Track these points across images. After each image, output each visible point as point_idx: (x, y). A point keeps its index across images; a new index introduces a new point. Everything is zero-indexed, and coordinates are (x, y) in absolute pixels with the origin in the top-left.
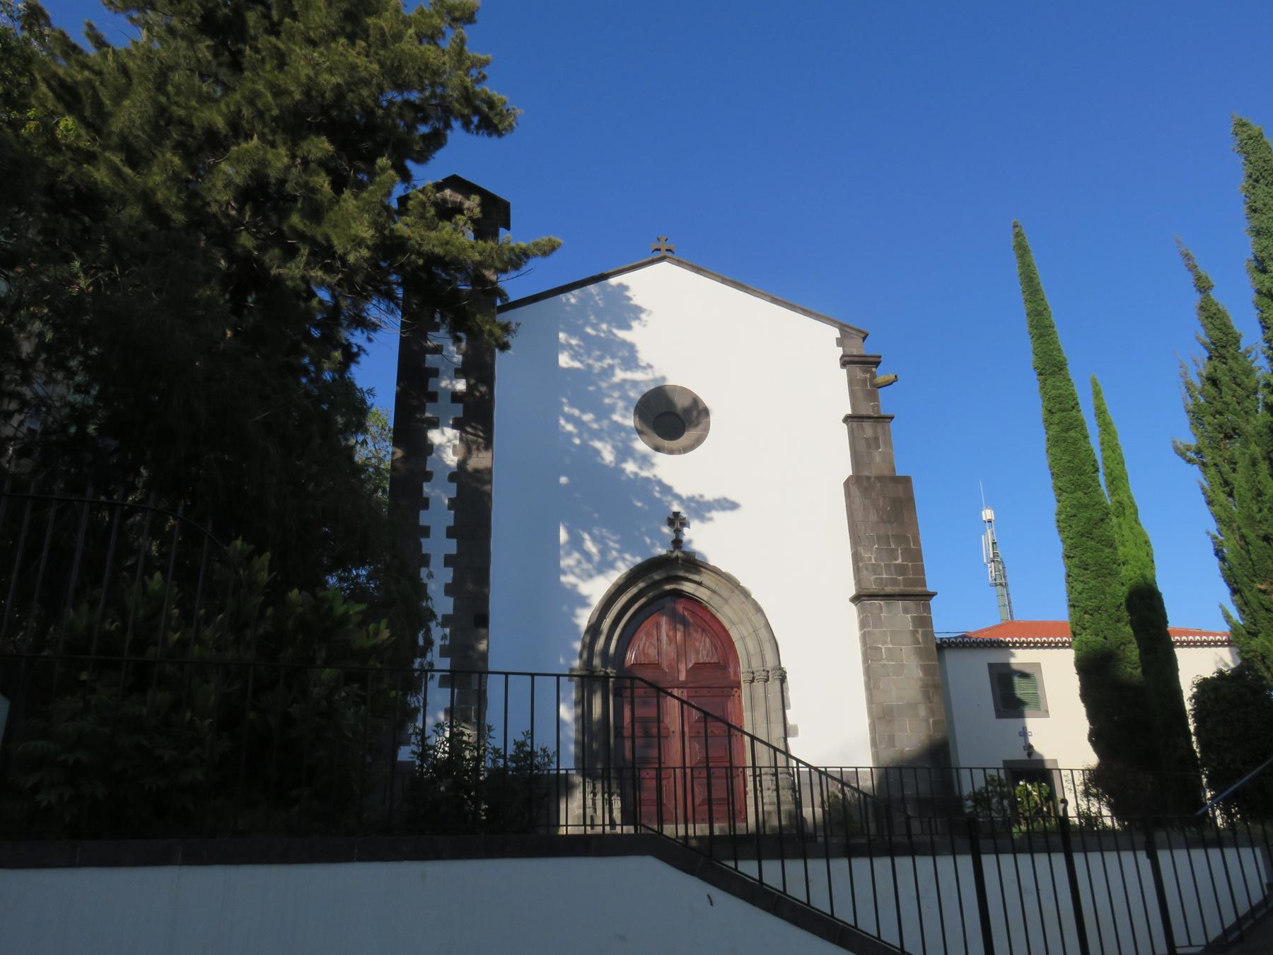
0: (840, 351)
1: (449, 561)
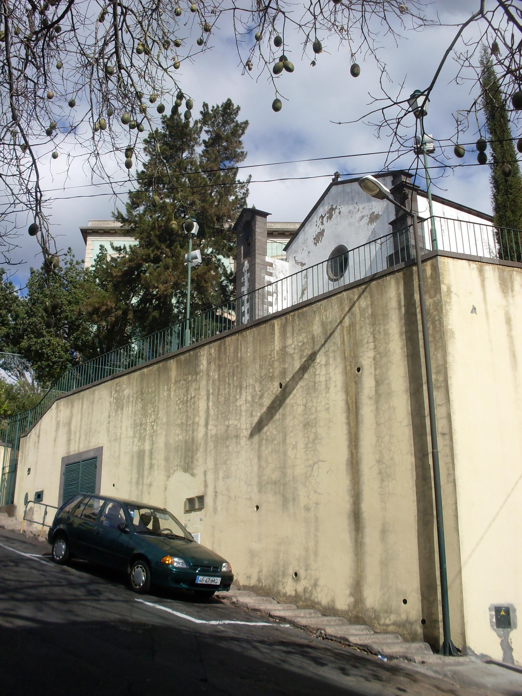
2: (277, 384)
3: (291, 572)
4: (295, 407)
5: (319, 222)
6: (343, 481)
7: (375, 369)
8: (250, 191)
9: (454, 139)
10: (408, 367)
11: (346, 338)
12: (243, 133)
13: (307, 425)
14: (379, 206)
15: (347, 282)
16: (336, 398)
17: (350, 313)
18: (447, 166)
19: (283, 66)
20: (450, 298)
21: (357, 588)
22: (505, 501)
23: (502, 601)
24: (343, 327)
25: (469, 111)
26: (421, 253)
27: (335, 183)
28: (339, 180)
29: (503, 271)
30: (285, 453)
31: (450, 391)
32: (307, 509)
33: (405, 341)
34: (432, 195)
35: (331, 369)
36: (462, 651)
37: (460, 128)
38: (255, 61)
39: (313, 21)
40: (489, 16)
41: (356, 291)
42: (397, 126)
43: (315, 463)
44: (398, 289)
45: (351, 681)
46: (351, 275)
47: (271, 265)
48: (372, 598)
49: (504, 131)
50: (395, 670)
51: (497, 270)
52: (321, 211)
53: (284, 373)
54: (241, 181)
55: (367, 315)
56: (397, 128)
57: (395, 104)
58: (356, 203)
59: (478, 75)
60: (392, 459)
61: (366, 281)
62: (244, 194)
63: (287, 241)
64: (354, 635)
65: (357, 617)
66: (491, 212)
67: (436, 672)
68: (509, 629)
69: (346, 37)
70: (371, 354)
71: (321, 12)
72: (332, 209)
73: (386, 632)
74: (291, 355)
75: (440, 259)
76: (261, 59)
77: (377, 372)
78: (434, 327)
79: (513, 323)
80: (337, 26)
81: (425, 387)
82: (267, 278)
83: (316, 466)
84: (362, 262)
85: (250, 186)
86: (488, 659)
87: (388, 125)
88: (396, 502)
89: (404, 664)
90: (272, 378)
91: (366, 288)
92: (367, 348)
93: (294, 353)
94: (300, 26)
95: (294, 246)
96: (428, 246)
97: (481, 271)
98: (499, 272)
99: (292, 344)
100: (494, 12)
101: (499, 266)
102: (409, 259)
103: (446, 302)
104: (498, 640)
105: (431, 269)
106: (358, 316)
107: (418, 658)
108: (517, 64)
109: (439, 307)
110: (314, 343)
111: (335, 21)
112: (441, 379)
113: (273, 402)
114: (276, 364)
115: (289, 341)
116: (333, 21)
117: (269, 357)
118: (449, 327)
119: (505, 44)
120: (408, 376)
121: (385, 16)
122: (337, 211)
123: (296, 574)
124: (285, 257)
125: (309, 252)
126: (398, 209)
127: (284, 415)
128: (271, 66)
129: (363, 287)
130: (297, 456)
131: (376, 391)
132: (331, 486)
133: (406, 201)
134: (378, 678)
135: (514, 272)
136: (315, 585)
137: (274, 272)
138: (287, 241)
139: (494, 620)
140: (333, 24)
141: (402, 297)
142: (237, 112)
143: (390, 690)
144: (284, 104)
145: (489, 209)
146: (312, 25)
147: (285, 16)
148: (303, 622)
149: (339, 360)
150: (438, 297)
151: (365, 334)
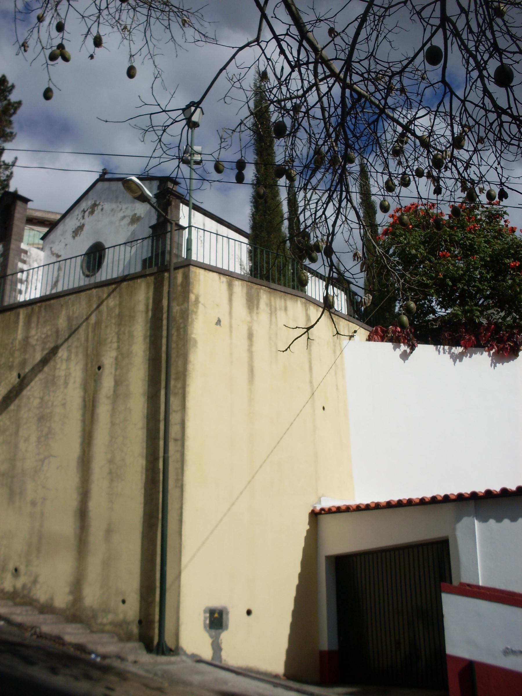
2: (15, 374)
3: (11, 567)
4: (32, 400)
5: (80, 216)
6: (72, 478)
7: (116, 369)
8: (15, 174)
9: (216, 155)
10: (149, 371)
11: (90, 335)
12: (15, 113)
13: (42, 418)
14: (141, 209)
15: (104, 278)
16: (74, 394)
17: (97, 312)
18: (205, 180)
19: (60, 54)
20: (197, 307)
21: (77, 585)
22: (229, 509)
23: (216, 603)
24: (89, 324)
25: (234, 131)
26: (174, 260)
27: (102, 178)
28: (106, 176)
29: (251, 288)
30: (16, 446)
31: (187, 399)
32: (34, 503)
33: (148, 345)
34: (193, 204)
35: (72, 364)
36: (176, 651)
37: (223, 145)
38: (31, 43)
39: (97, 15)
40: (263, 45)
41: (106, 290)
42: (163, 133)
43: (45, 458)
44: (147, 293)
45: (60, 681)
46: (106, 273)
47: (26, 252)
48: (91, 596)
49: (269, 155)
50: (106, 669)
51: (245, 287)
52: (84, 205)
53: (23, 363)
54: (7, 162)
55: (113, 315)
56: (162, 135)
57: (164, 111)
58: (120, 202)
59: (247, 98)
60: (123, 460)
61: (117, 280)
62: (7, 176)
63: (45, 230)
64: (69, 634)
65: (75, 615)
66: (247, 229)
67: (147, 671)
68: (220, 631)
69: (128, 38)
70: (114, 354)
71: (107, 7)
72: (95, 205)
73: (102, 631)
74: (34, 347)
75: (193, 269)
76: (39, 43)
77: (118, 373)
78: (179, 334)
79: (255, 339)
80: (120, 24)
81: (163, 392)
82: (20, 265)
83: (46, 461)
84: (116, 263)
85: (15, 169)
86: (198, 659)
87: (154, 130)
88: (122, 504)
89: (116, 664)
90: (11, 368)
91: (116, 288)
92: (110, 347)
93: (36, 345)
94: (83, 17)
95: (51, 236)
96: (184, 255)
97: (230, 286)
98: (247, 289)
99: (35, 335)
100: (268, 42)
101: (248, 283)
102: (164, 265)
103: (193, 311)
104: (209, 641)
105: (183, 277)
106: (105, 314)
107: (131, 658)
108: (283, 95)
109: (186, 316)
110: (57, 337)
111: (119, 19)
112: (179, 385)
113: (10, 392)
114: (17, 354)
115: (33, 332)
116: (117, 18)
117: (11, 346)
118: (193, 336)
119: (275, 74)
120: (147, 379)
121: (169, 25)
122: (100, 207)
123: (16, 570)
124: (41, 246)
125: (66, 245)
126: (159, 216)
127: (19, 407)
128: (48, 52)
129: (114, 286)
130: (29, 449)
131: (115, 391)
132: (59, 482)
133: (169, 208)
134: (88, 677)
135: (262, 291)
136: (35, 582)
137: (28, 259)
138: (45, 230)
139: (208, 622)
140: (117, 21)
141: (151, 301)
142: (11, 90)
143: (100, 689)
144: (56, 93)
145: (246, 226)
146: (94, 18)
147: (69, 4)
148: (18, 619)
149: (81, 356)
150: (186, 305)
151: (110, 333)
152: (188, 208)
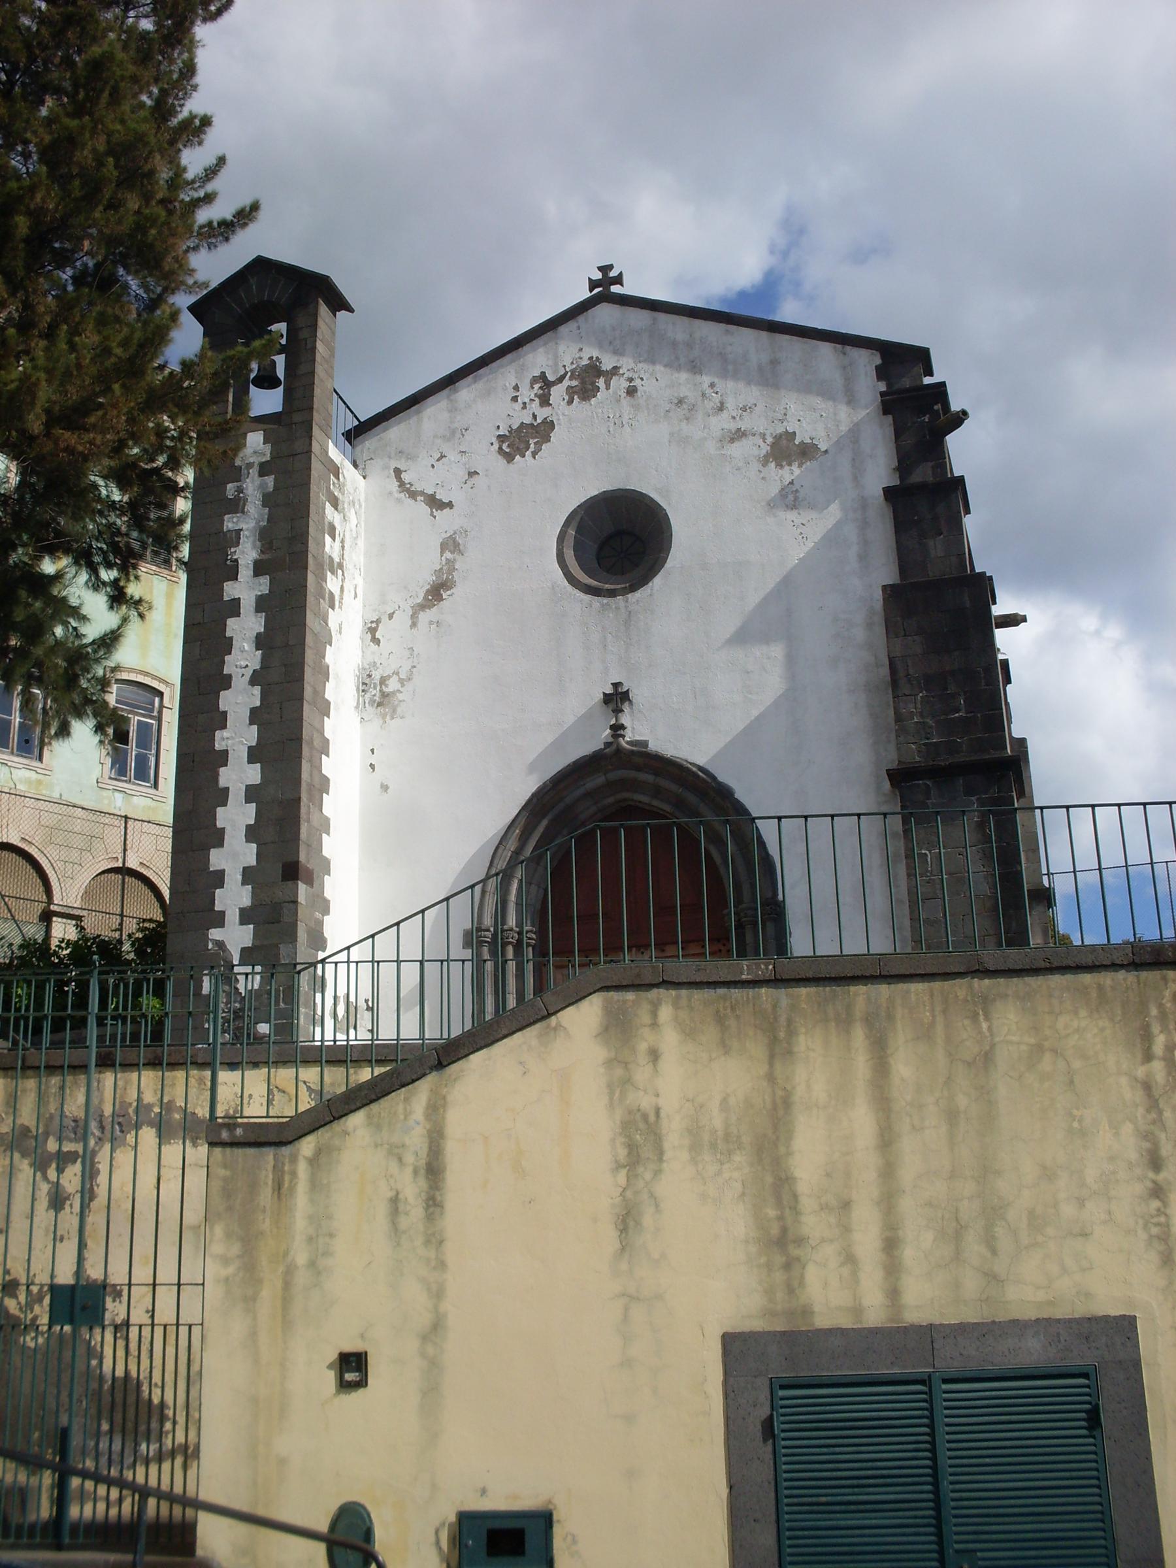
0: (882, 386)
1: (252, 794)
122: (619, 384)
152: (1015, 735)
